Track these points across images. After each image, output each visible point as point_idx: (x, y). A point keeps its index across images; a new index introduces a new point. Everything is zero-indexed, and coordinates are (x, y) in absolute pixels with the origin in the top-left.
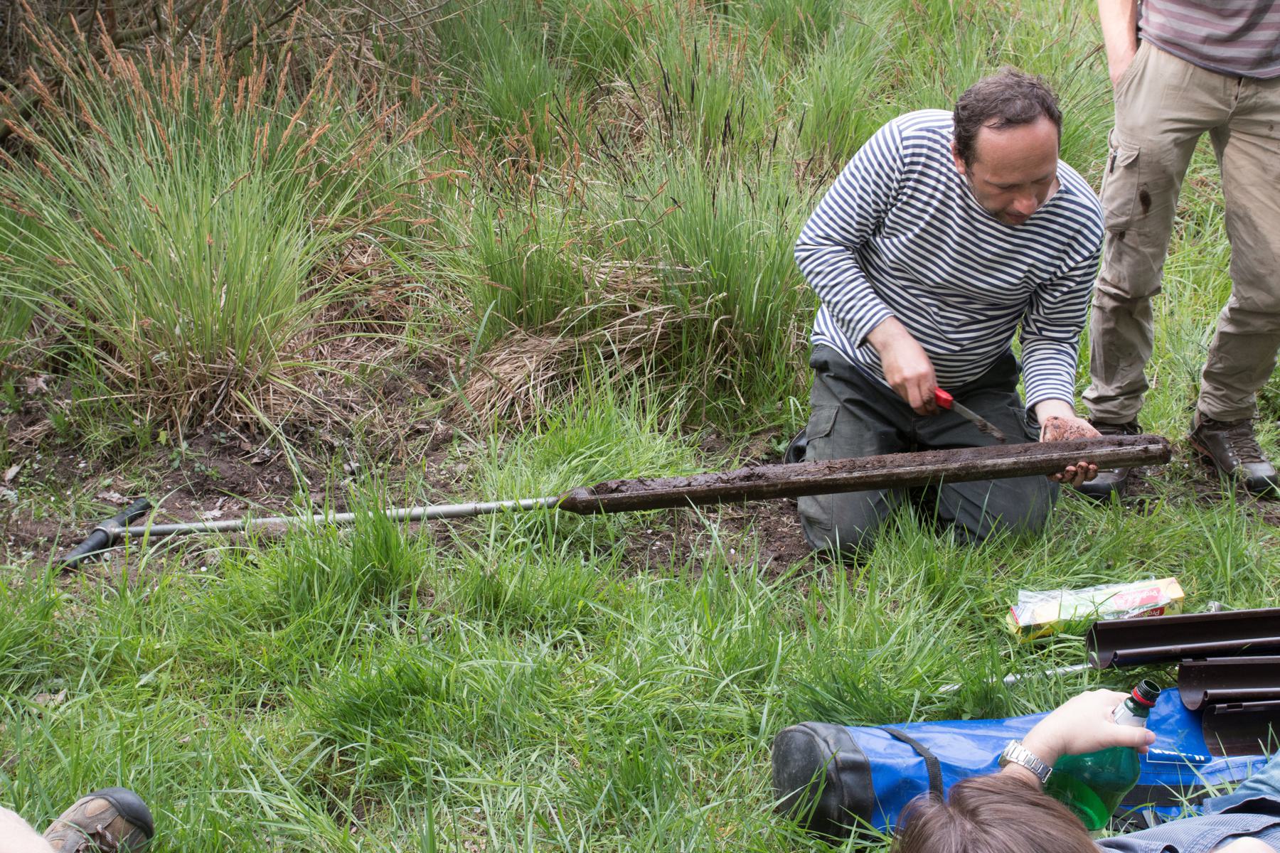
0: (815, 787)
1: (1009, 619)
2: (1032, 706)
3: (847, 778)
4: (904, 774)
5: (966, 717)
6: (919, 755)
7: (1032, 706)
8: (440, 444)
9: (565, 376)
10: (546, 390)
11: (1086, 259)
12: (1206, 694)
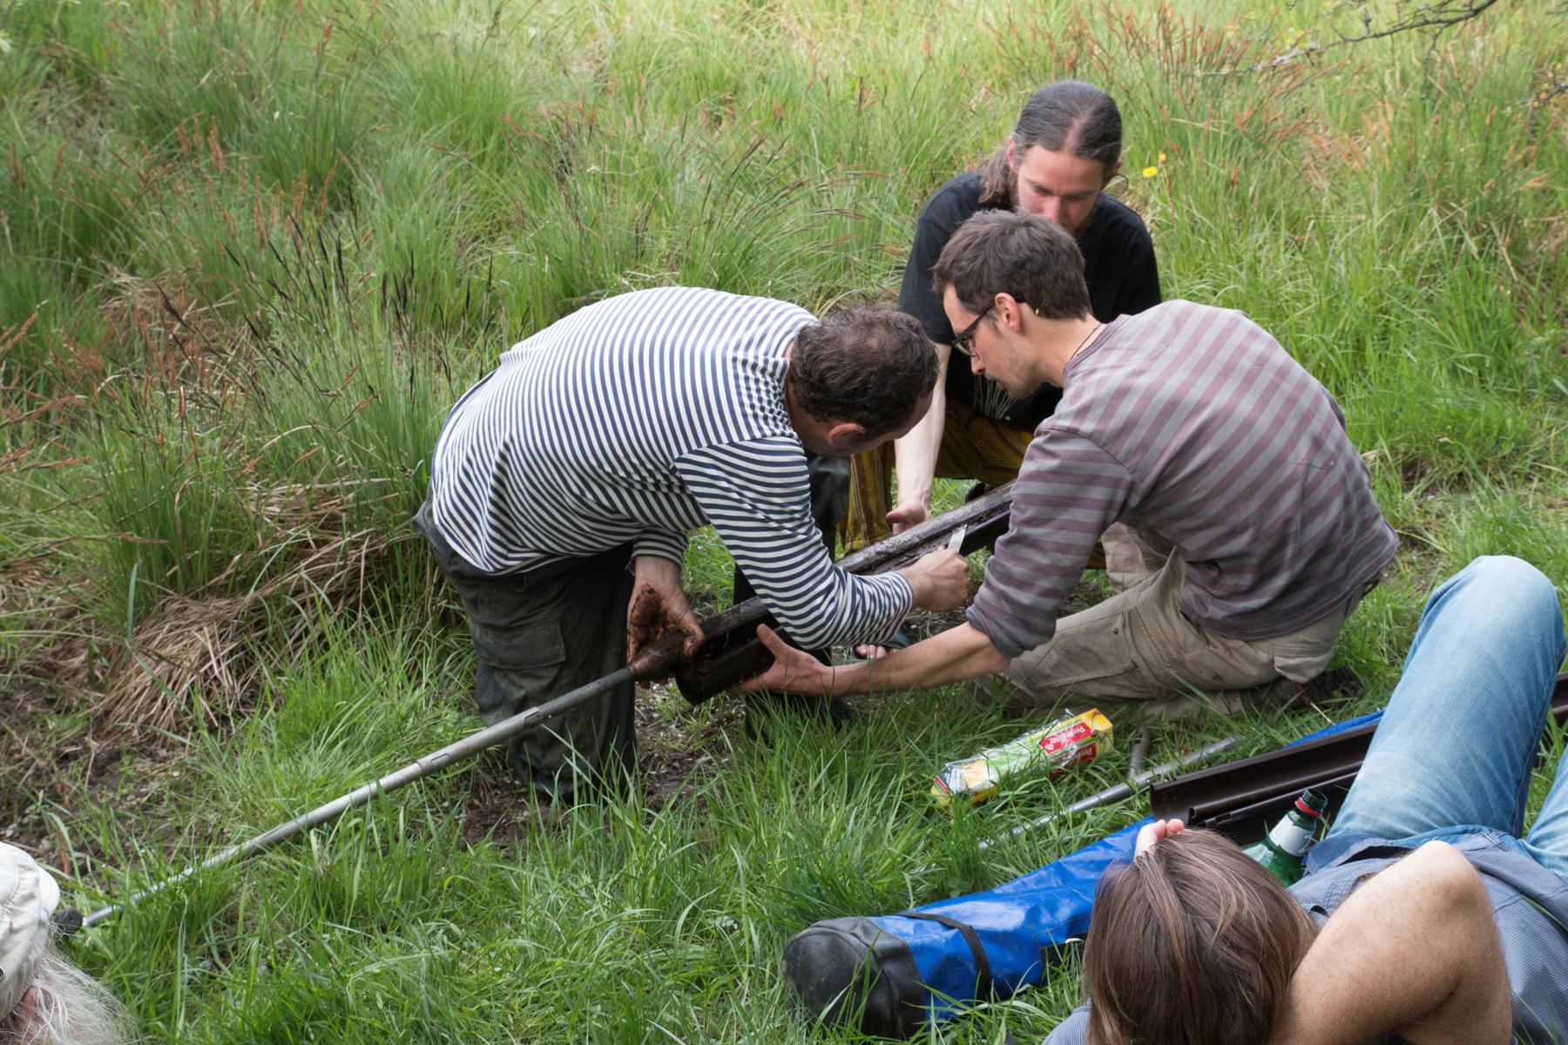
0: (859, 986)
1: (934, 791)
2: (1011, 870)
3: (891, 968)
4: (947, 950)
5: (954, 895)
6: (951, 928)
7: (1011, 870)
8: (102, 769)
9: (256, 638)
10: (229, 667)
11: (754, 439)
12: (1192, 812)
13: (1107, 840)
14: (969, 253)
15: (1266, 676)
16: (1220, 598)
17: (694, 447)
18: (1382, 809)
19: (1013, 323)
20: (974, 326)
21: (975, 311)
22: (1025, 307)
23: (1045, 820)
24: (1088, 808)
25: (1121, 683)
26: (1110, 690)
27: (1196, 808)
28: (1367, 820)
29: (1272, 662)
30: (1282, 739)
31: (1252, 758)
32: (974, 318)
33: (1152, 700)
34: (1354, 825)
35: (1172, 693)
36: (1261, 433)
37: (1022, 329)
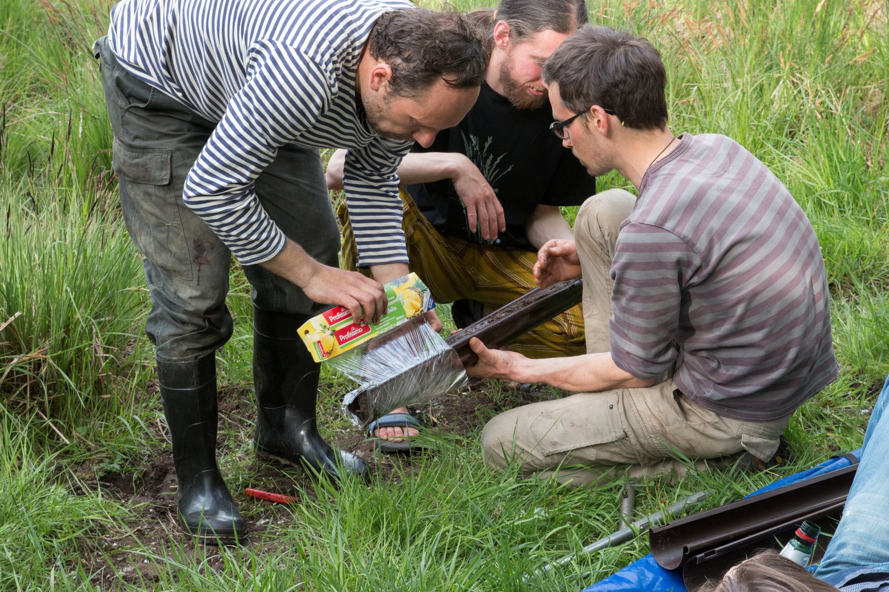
12: (686, 549)
13: (618, 574)
14: (575, 64)
15: (731, 447)
16: (719, 384)
17: (274, 39)
18: (869, 538)
19: (603, 130)
20: (571, 121)
21: (573, 110)
22: (614, 119)
23: (567, 559)
24: (601, 548)
25: (613, 449)
26: (604, 455)
27: (689, 546)
28: (857, 547)
29: (740, 437)
30: (742, 491)
31: (723, 505)
32: (572, 115)
33: (637, 466)
34: (847, 553)
35: (657, 458)
36: (639, 335)
37: (609, 134)
